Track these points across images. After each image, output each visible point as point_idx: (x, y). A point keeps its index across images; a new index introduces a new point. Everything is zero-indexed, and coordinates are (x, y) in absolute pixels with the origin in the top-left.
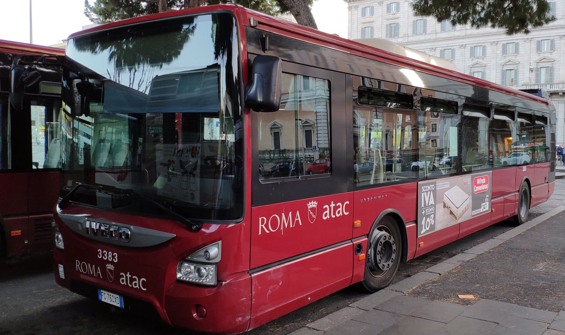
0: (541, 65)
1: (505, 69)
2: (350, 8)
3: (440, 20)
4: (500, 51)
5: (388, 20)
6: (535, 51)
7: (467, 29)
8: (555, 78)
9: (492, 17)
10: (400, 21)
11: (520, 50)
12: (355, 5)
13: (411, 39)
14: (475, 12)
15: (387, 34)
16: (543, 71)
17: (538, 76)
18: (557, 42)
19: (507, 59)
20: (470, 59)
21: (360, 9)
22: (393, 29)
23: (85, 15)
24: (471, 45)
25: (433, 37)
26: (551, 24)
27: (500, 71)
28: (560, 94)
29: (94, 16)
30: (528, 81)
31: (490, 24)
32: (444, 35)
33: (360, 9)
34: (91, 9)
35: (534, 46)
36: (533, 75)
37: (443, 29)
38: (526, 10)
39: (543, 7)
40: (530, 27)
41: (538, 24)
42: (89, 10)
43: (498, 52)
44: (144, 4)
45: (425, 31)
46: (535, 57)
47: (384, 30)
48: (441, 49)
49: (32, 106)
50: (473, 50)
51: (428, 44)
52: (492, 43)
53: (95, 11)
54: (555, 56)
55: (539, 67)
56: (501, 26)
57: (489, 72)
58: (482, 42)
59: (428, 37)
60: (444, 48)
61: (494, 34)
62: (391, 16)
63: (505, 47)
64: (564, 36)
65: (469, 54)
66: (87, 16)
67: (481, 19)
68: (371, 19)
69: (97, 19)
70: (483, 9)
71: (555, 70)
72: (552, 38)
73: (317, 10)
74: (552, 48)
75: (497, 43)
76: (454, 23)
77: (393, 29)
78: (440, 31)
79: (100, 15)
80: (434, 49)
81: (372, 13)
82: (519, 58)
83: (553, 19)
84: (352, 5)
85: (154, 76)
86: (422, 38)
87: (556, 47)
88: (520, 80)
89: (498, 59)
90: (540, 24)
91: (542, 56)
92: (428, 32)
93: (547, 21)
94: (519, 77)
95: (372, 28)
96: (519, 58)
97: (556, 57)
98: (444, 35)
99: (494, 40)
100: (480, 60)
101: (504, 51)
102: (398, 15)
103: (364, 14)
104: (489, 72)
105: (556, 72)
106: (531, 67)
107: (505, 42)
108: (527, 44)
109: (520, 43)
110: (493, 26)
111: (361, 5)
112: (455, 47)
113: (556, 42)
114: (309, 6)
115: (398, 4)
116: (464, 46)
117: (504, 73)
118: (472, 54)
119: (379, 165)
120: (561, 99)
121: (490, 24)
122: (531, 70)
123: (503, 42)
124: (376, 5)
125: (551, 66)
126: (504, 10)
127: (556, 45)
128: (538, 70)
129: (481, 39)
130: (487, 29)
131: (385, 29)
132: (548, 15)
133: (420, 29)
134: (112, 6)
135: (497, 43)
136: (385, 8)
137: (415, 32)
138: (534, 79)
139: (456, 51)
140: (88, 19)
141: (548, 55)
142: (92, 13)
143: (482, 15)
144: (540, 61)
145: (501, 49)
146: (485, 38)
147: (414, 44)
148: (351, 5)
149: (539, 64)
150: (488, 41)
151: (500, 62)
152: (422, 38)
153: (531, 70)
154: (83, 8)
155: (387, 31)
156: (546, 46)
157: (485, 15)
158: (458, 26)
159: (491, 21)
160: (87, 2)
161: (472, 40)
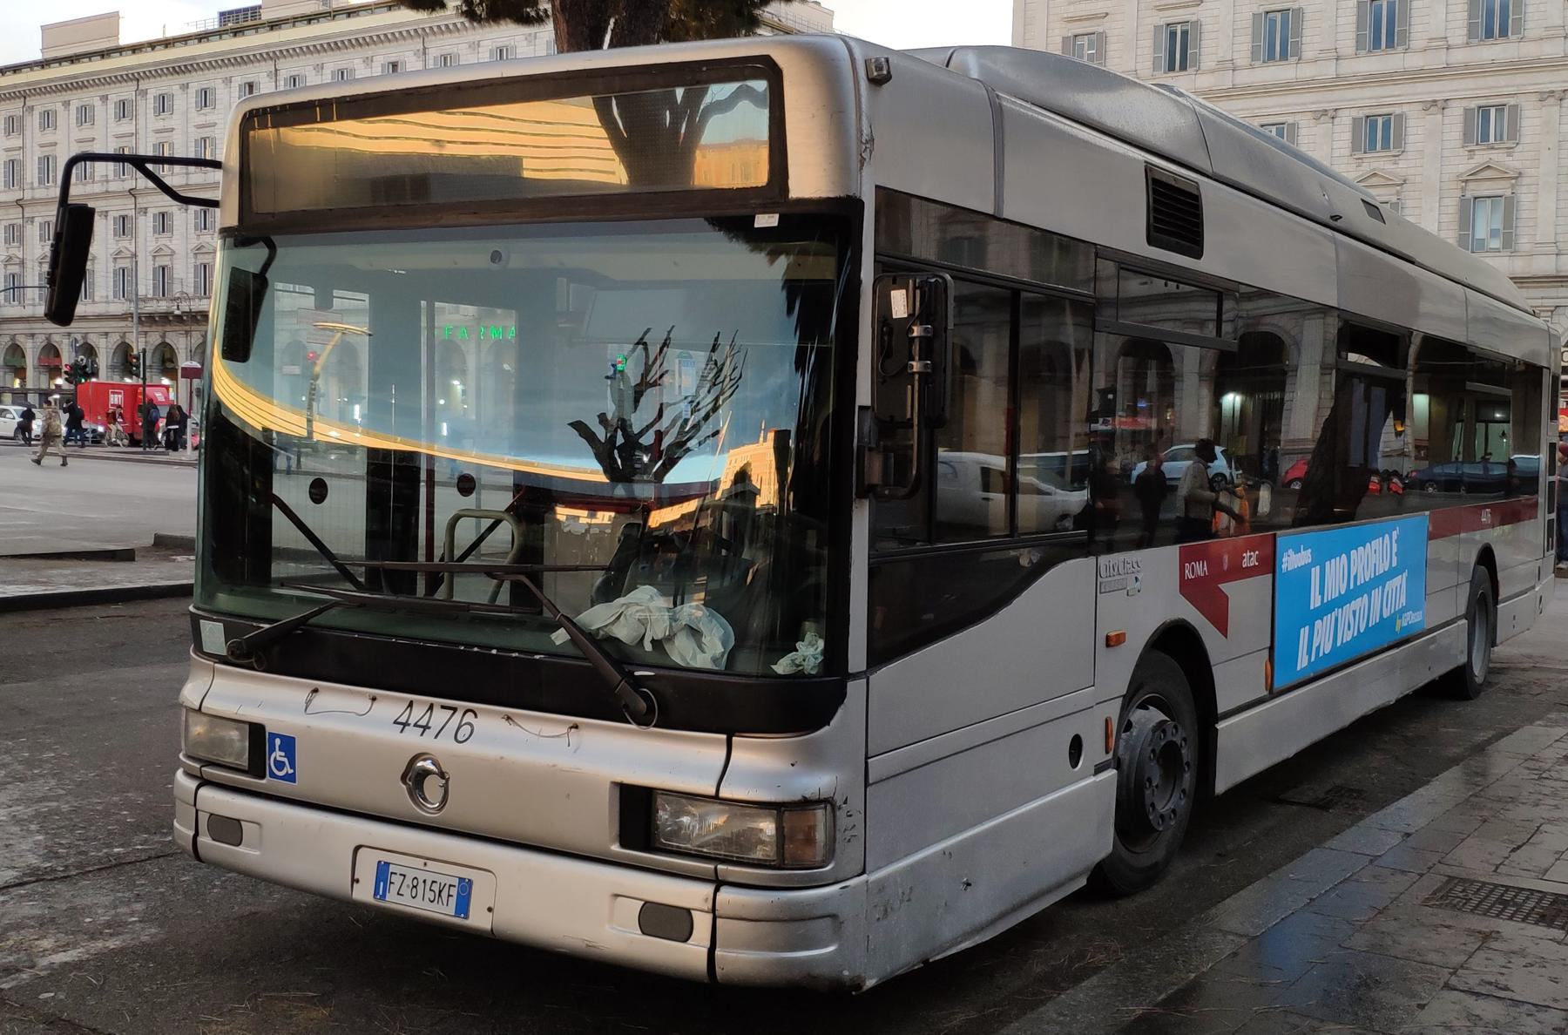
0: (1475, 189)
1: (1469, 195)
5: (1071, 20)
15: (1156, 60)
25: (1329, 70)
47: (1147, 44)
57: (1530, 197)
58: (1506, 91)
64: (1561, 96)
78: (1246, 62)
80: (1330, 115)
85: (90, 205)
100: (1497, 157)
104: (1530, 197)
112: (1405, 108)
116: (1437, 106)
117: (1467, 210)
119: (1078, 371)
125: (1508, 193)
131: (1150, 43)
146: (1520, 79)
149: (1471, 185)
150: (1531, 89)
155: (1156, 48)
161: (1470, 83)
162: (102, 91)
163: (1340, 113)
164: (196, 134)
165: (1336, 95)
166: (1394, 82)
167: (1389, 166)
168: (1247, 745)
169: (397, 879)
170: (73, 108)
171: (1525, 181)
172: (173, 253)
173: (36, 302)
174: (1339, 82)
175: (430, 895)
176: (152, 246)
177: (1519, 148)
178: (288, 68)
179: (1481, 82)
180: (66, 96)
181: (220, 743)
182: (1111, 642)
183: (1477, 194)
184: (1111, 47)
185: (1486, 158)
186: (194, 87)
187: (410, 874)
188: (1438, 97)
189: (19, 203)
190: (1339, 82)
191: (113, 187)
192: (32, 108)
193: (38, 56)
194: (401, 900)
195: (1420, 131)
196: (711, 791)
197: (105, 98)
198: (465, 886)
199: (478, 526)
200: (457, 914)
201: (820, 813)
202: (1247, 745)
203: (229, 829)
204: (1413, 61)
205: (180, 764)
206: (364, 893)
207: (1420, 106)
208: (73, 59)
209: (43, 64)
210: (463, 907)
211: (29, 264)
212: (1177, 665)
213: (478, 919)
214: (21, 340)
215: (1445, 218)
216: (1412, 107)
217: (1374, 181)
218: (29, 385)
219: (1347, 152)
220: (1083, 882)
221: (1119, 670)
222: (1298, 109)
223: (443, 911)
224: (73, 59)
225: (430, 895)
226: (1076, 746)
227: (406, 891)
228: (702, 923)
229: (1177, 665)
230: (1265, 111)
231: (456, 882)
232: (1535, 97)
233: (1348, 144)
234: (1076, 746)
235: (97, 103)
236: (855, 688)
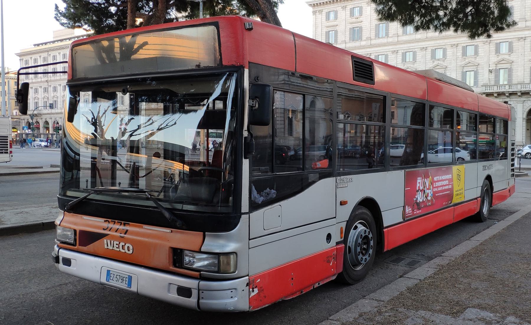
0: (500, 66)
1: (465, 70)
2: (314, 13)
3: (404, 24)
4: (460, 54)
5: (327, 27)
6: (494, 53)
7: (431, 33)
8: (514, 78)
9: (456, 21)
10: (363, 25)
11: (480, 52)
12: (319, 9)
13: (373, 42)
14: (438, 17)
15: (350, 38)
16: (502, 72)
17: (497, 77)
18: (516, 45)
19: (467, 61)
21: (324, 13)
22: (356, 33)
23: (55, 19)
24: (432, 48)
26: (512, 28)
27: (460, 72)
28: (519, 94)
29: (65, 20)
30: (488, 82)
31: (452, 28)
32: (405, 38)
33: (324, 13)
34: (60, 13)
35: (493, 48)
36: (492, 76)
37: (405, 33)
38: (486, 15)
39: (505, 12)
40: (492, 32)
41: (500, 29)
42: (59, 15)
43: (458, 54)
44: (113, 9)
45: (387, 35)
46: (494, 59)
47: (348, 33)
48: (402, 51)
50: (433, 52)
51: (390, 47)
52: (393, 52)
53: (64, 16)
54: (513, 57)
55: (498, 68)
56: (463, 31)
59: (390, 40)
60: (406, 51)
61: (427, 39)
62: (354, 20)
63: (464, 49)
65: (430, 57)
66: (57, 20)
67: (444, 24)
68: (335, 23)
69: (66, 23)
70: (445, 14)
71: (514, 71)
72: (510, 40)
73: (297, 12)
74: (511, 50)
75: (457, 45)
76: (417, 29)
77: (356, 33)
78: (401, 34)
79: (70, 19)
81: (336, 18)
82: (478, 60)
83: (514, 23)
84: (317, 9)
86: (385, 41)
87: (514, 49)
88: (479, 81)
89: (458, 61)
90: (502, 29)
91: (501, 57)
92: (390, 35)
93: (508, 26)
94: (479, 78)
95: (336, 32)
96: (478, 60)
97: (514, 59)
98: (405, 38)
99: (454, 43)
101: (464, 53)
102: (360, 19)
103: (328, 18)
104: (482, 71)
105: (514, 74)
106: (490, 68)
107: (465, 45)
108: (486, 47)
110: (456, 31)
111: (350, 5)
112: (416, 50)
113: (514, 44)
114: (275, 9)
116: (425, 49)
118: (433, 56)
120: (519, 99)
121: (452, 28)
122: (490, 71)
123: (463, 45)
124: (364, 5)
126: (466, 15)
127: (514, 47)
128: (497, 71)
129: (441, 41)
130: (451, 32)
131: (348, 33)
132: (510, 20)
133: (382, 33)
134: (80, 11)
135: (457, 45)
136: (348, 12)
137: (377, 36)
138: (494, 80)
140: (58, 23)
141: (507, 57)
142: (62, 18)
143: (445, 20)
144: (499, 62)
145: (430, 55)
146: (446, 41)
147: (376, 47)
148: (315, 10)
149: (498, 65)
150: (449, 43)
151: (460, 64)
152: (385, 41)
153: (490, 71)
154: (53, 13)
156: (504, 48)
157: (448, 20)
158: (421, 31)
159: (454, 26)
160: (57, 7)
161: (433, 42)
162: (31, 56)
165: (398, 46)
166: (413, 43)
167: (412, 66)
169: (112, 275)
170: (61, 54)
171: (448, 69)
172: (38, 99)
173: (16, 112)
174: (398, 43)
176: (52, 95)
178: (52, 53)
179: (436, 42)
180: (59, 51)
181: (66, 236)
182: (343, 203)
184: (339, 34)
186: (62, 53)
187: (116, 274)
188: (424, 46)
189: (47, 81)
190: (398, 43)
191: (43, 80)
192: (50, 55)
193: (52, 40)
195: (451, 53)
196: (197, 250)
197: (59, 53)
198: (130, 278)
199: (120, 170)
201: (232, 256)
203: (67, 262)
204: (363, 43)
205: (55, 243)
206: (104, 280)
208: (61, 40)
209: (54, 42)
210: (130, 285)
211: (50, 99)
213: (134, 289)
214: (48, 120)
217: (438, 67)
218: (50, 132)
219: (401, 62)
220: (334, 278)
221: (345, 213)
222: (512, 37)
223: (123, 286)
224: (61, 40)
226: (329, 237)
227: (115, 279)
228: (195, 293)
230: (499, 38)
233: (401, 60)
234: (329, 237)
235: (30, 59)
236: (244, 218)
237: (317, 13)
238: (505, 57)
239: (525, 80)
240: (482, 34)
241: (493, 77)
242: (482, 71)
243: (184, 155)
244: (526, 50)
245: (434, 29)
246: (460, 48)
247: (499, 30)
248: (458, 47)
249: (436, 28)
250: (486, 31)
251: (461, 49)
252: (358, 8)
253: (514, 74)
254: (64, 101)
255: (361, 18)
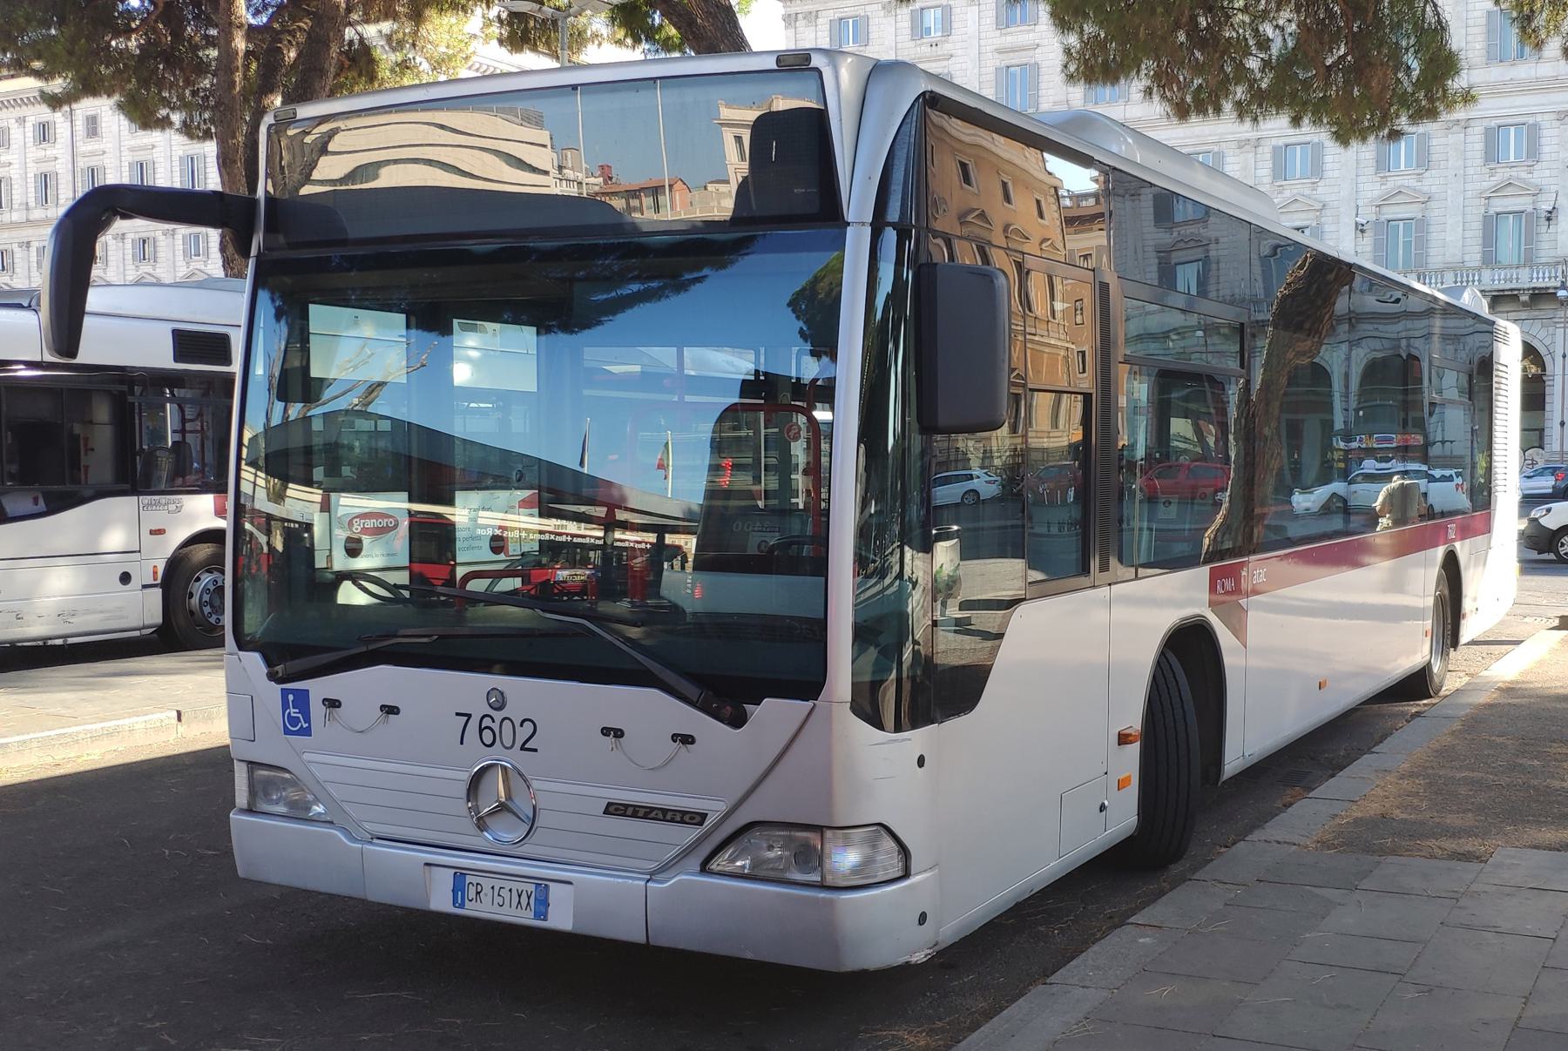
0: (1499, 205)
5: (1000, 51)
6: (1372, 170)
8: (1432, 252)
11: (1328, 166)
14: (1242, 73)
20: (1485, 170)
28: (1524, 298)
49: (312, 307)
58: (1211, 139)
70: (1266, 64)
71: (1432, 229)
84: (798, 9)
87: (1434, 157)
97: (1434, 189)
102: (947, 48)
104: (1333, 228)
105: (1435, 236)
109: (1545, 124)
115: (947, 11)
123: (1274, 142)
125: (1420, 216)
132: (1457, 84)
139: (1545, 133)
149: (1385, 209)
150: (1230, 137)
153: (1360, 229)
163: (1472, 123)
164: (128, 158)
168: (1248, 736)
171: (1328, 212)
175: (498, 900)
177: (1427, 174)
183: (1499, 210)
185: (1507, 175)
194: (483, 908)
200: (537, 916)
202: (1248, 736)
206: (441, 901)
207: (1553, 116)
212: (1191, 658)
215: (1468, 234)
216: (1546, 117)
217: (1399, 199)
225: (498, 900)
229: (1191, 658)
231: (531, 888)
232: (1234, 145)
237: (801, 23)
238: (1406, 183)
239: (1467, 258)
240: (1374, 129)
241: (1369, 248)
242: (1333, 228)
243: (1070, 445)
244: (1469, 163)
245: (1235, 115)
246: (1266, 152)
247: (1421, 118)
248: (1260, 150)
249: (1242, 110)
250: (1385, 118)
251: (1268, 156)
252: (939, 11)
253: (1433, 236)
254: (1347, 376)
255: (947, 46)
